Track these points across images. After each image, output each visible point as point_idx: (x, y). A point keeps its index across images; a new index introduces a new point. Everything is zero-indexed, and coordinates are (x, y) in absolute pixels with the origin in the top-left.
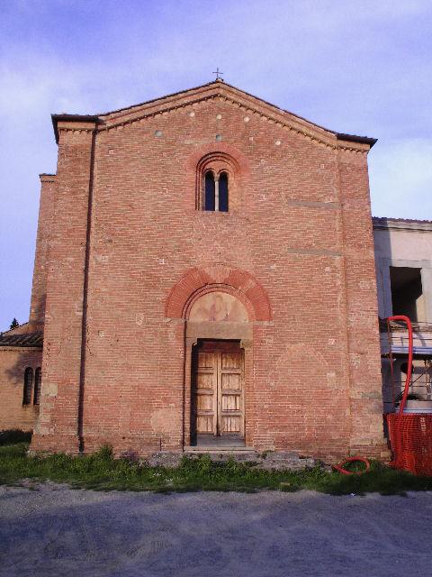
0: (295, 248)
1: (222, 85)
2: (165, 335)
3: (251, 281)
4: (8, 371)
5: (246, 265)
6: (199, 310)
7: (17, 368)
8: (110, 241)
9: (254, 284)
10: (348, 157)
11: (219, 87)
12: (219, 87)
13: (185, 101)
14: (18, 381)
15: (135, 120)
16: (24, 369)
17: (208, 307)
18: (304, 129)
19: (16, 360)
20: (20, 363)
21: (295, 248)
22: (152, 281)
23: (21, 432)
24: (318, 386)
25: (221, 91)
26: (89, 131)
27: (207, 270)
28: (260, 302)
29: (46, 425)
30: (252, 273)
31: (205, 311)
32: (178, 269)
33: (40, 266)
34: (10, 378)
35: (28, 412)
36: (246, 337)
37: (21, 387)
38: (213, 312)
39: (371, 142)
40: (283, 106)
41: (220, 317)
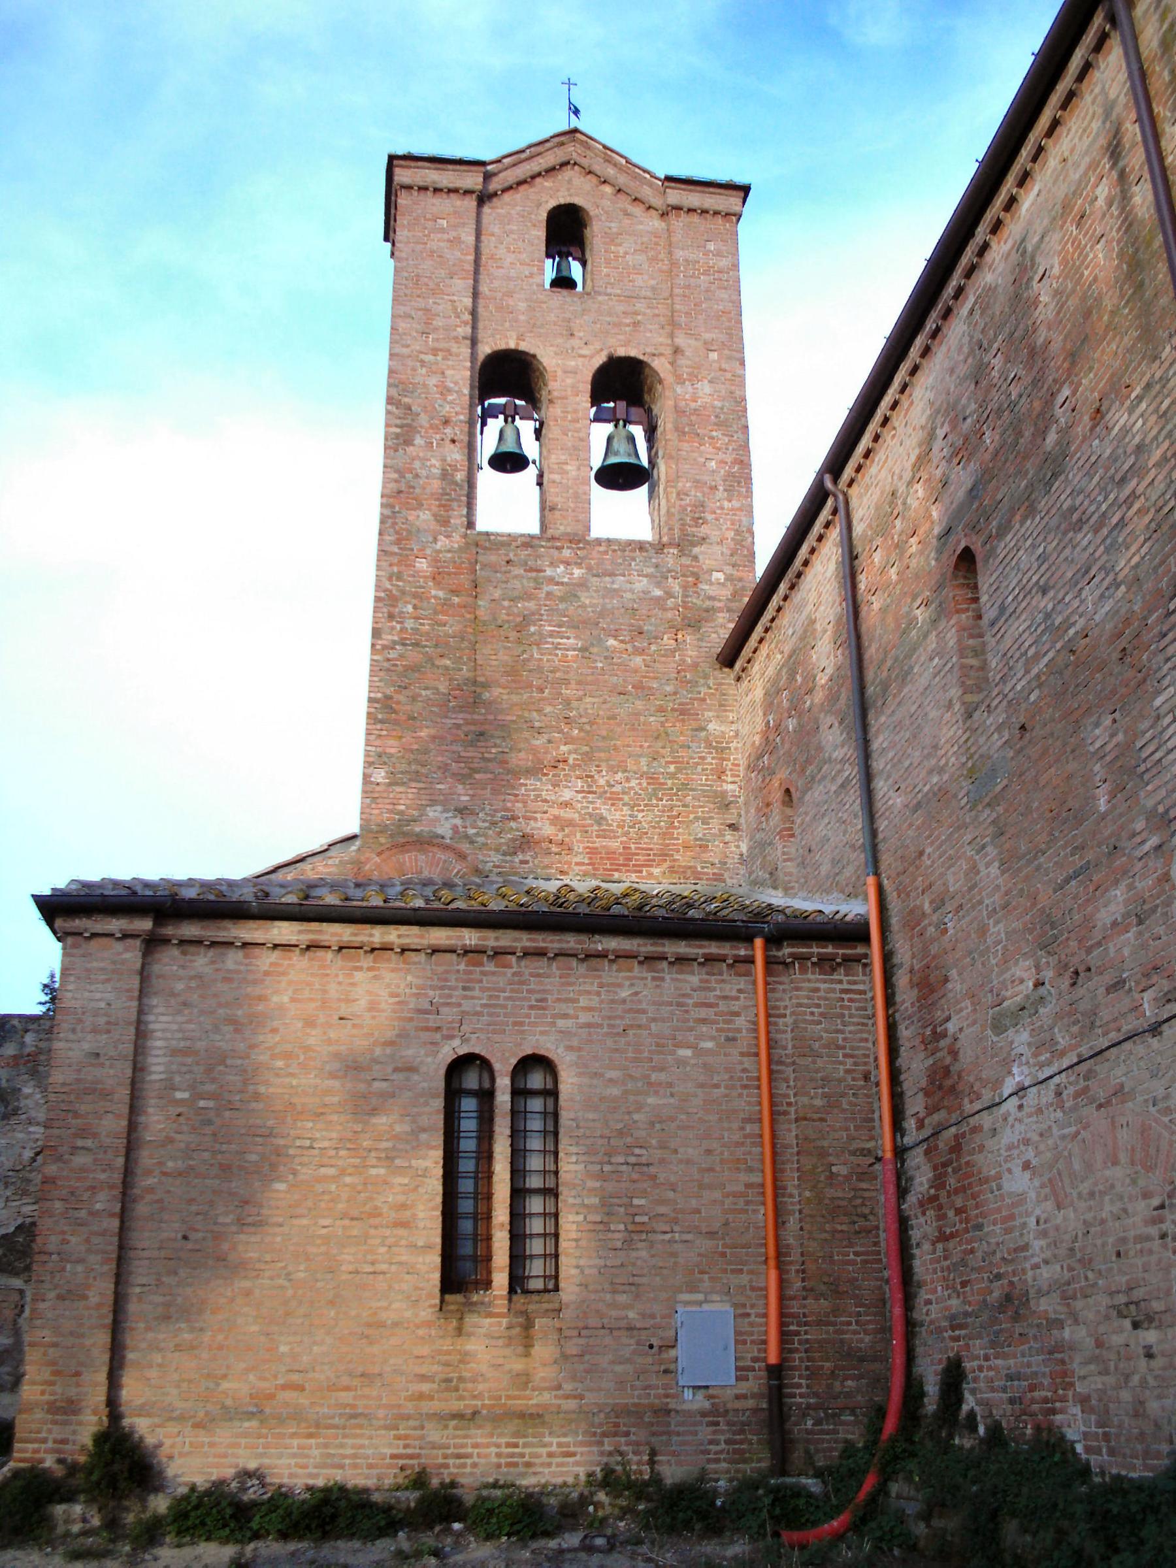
33: (405, 560)
35: (473, 1346)
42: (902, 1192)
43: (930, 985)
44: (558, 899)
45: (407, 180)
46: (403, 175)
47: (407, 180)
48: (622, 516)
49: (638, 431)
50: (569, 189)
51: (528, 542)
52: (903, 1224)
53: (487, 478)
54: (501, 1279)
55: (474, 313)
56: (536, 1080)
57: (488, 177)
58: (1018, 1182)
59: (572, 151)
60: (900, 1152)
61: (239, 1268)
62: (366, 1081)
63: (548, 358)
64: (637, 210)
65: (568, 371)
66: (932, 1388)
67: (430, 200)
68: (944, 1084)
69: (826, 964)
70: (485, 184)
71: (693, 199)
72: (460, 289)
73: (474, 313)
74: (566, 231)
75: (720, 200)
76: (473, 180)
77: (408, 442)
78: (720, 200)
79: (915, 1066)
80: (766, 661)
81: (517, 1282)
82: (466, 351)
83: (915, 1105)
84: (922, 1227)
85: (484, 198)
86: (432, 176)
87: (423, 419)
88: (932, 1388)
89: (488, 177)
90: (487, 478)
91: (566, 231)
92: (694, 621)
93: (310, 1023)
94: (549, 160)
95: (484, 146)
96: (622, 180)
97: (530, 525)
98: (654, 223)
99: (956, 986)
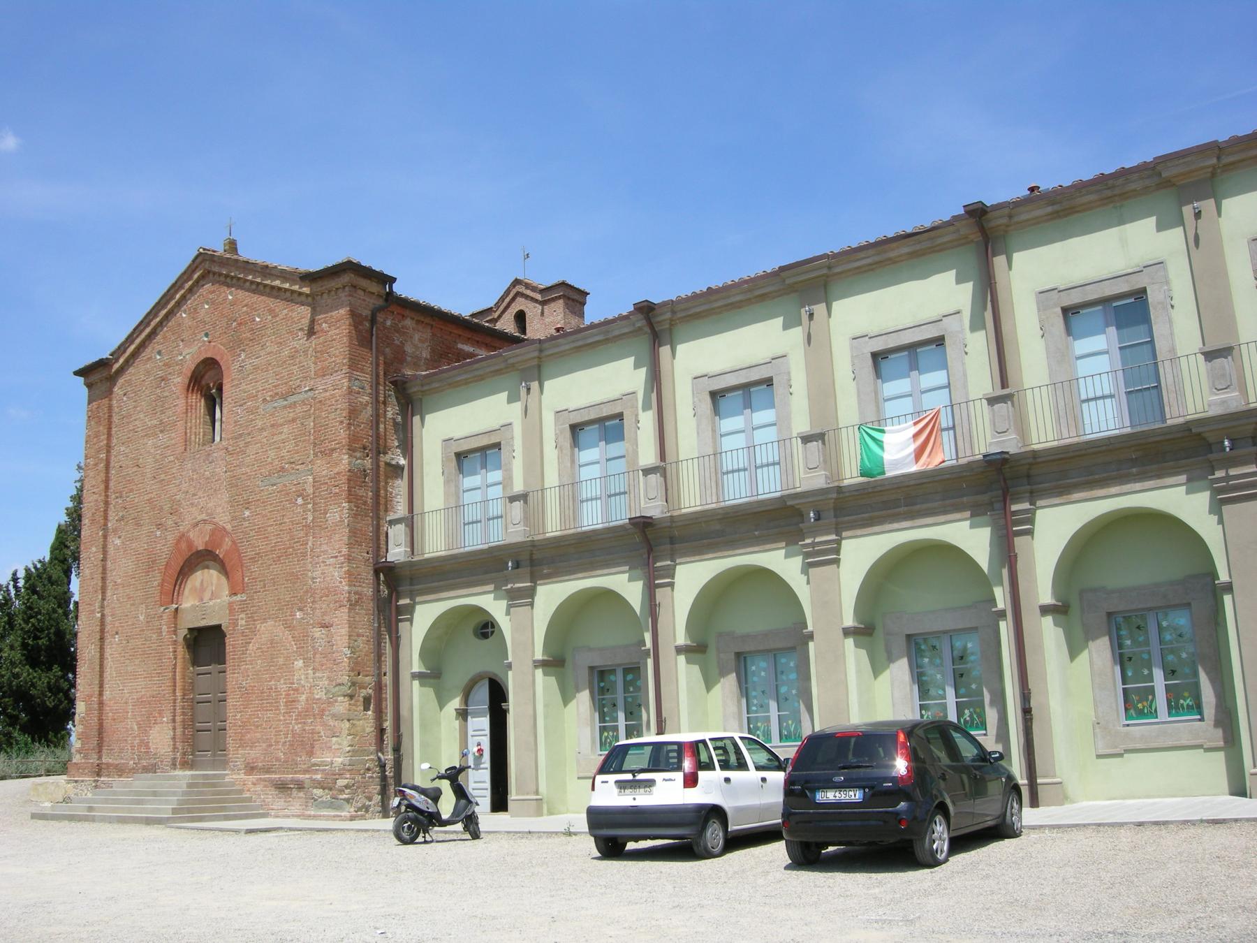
30: (229, 527)
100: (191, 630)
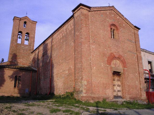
0: (129, 51)
1: (114, 8)
2: (108, 70)
3: (122, 58)
4: (9, 76)
5: (121, 53)
6: (113, 64)
7: (12, 75)
8: (94, 42)
9: (123, 59)
10: (136, 31)
11: (113, 8)
12: (113, 8)
13: (107, 9)
14: (13, 80)
15: (97, 11)
16: (14, 76)
17: (115, 63)
18: (128, 23)
19: (12, 73)
20: (13, 74)
21: (129, 51)
22: (104, 55)
23: (14, 97)
24: (135, 87)
25: (113, 9)
26: (88, 10)
27: (115, 54)
28: (124, 63)
29: (85, 93)
31: (114, 64)
32: (109, 52)
33: (13, 44)
34: (10, 79)
35: (15, 90)
36: (122, 72)
37: (13, 82)
38: (115, 65)
39: (139, 29)
40: (125, 17)
41: (117, 66)
42: (37, 84)
43: (39, 74)
44: (20, 67)
45: (15, 18)
46: (15, 18)
47: (15, 18)
48: (26, 43)
49: (28, 37)
50: (26, 20)
51: (20, 44)
52: (37, 85)
53: (18, 39)
54: (17, 87)
55: (19, 28)
56: (16, 77)
57: (21, 19)
58: (42, 84)
59: (26, 18)
60: (37, 82)
61: (2, 86)
62: (11, 77)
63: (23, 32)
64: (30, 22)
65: (24, 32)
66: (37, 93)
67: (17, 20)
68: (40, 79)
69: (35, 73)
70: (20, 19)
71: (34, 22)
72: (18, 26)
73: (19, 28)
74: (25, 23)
75: (35, 23)
76: (20, 19)
77: (14, 37)
78: (35, 23)
79: (38, 78)
80: (34, 54)
81: (18, 87)
82: (18, 31)
83: (38, 80)
84: (38, 85)
85: (20, 20)
86: (17, 18)
87: (15, 35)
88: (37, 93)
89: (21, 19)
90: (18, 39)
91: (25, 23)
92: (30, 50)
93: (8, 73)
94: (25, 18)
95: (20, 16)
96: (29, 20)
97: (20, 43)
98: (31, 23)
99: (41, 75)
100: (114, 71)
